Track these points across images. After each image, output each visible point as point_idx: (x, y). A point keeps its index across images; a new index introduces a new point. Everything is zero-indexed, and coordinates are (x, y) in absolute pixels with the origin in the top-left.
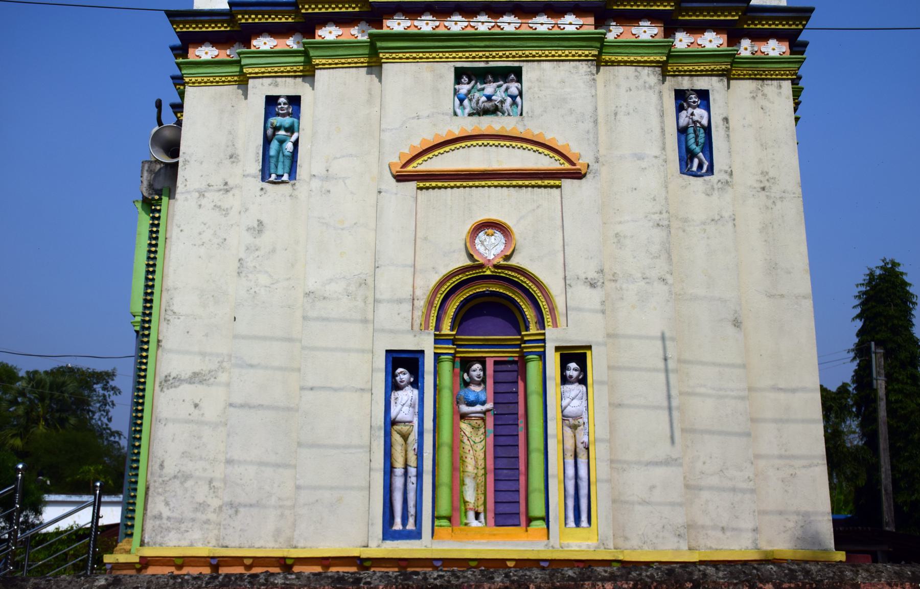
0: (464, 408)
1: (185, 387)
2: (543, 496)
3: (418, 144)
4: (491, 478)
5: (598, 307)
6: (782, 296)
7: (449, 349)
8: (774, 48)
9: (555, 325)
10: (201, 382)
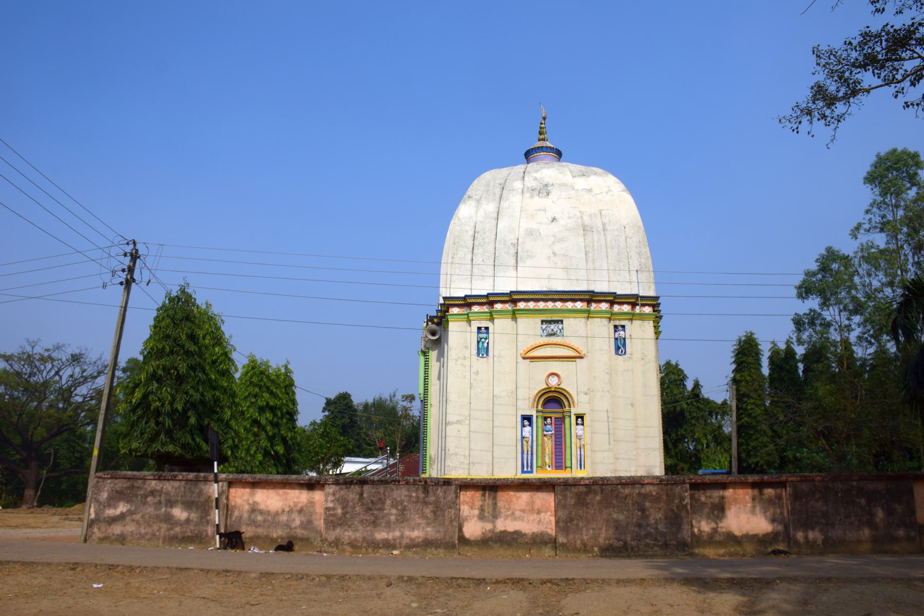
0: (545, 433)
6: (648, 395)
7: (541, 414)
8: (648, 310)
9: (574, 407)
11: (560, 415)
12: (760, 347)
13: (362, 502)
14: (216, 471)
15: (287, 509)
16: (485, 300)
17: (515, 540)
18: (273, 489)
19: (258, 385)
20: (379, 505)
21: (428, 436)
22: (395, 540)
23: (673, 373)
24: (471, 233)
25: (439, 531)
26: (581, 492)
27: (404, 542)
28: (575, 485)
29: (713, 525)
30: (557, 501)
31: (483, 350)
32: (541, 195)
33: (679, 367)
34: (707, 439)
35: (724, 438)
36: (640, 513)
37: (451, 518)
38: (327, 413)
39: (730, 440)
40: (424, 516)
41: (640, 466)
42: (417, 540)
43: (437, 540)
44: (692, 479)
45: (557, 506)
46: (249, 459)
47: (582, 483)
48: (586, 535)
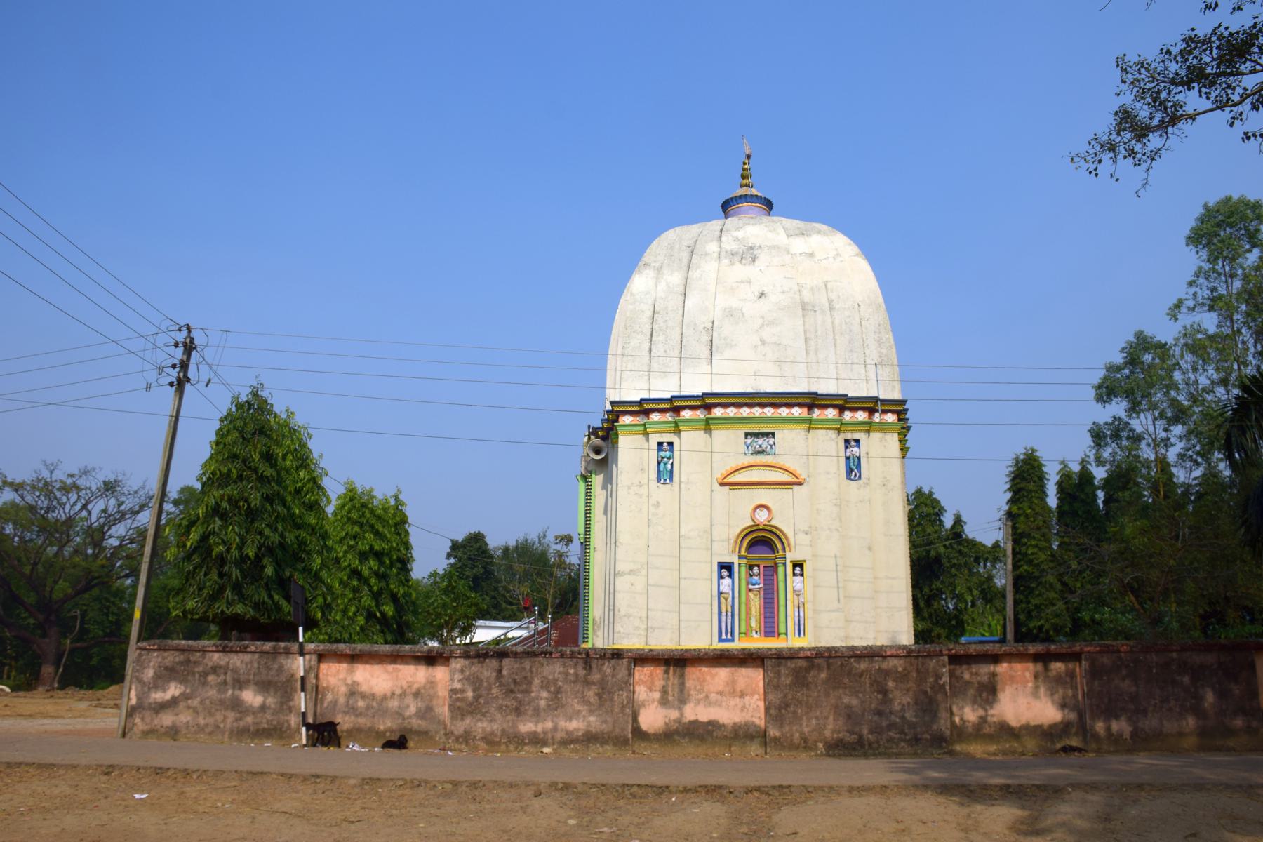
0: (751, 587)
3: (729, 468)
4: (762, 617)
6: (891, 535)
7: (744, 561)
8: (891, 418)
9: (790, 551)
11: (770, 563)
12: (1044, 469)
13: (501, 682)
14: (301, 639)
15: (398, 692)
16: (667, 406)
17: (710, 733)
20: (525, 686)
22: (545, 733)
23: (926, 505)
24: (649, 314)
25: (605, 722)
26: (800, 668)
27: (559, 736)
29: (981, 712)
30: (767, 681)
31: (665, 474)
32: (744, 261)
33: (934, 496)
34: (972, 596)
36: (880, 696)
38: (452, 561)
39: (1004, 596)
40: (585, 701)
43: (603, 733)
44: (952, 649)
46: (346, 623)
47: (801, 655)
48: (807, 726)
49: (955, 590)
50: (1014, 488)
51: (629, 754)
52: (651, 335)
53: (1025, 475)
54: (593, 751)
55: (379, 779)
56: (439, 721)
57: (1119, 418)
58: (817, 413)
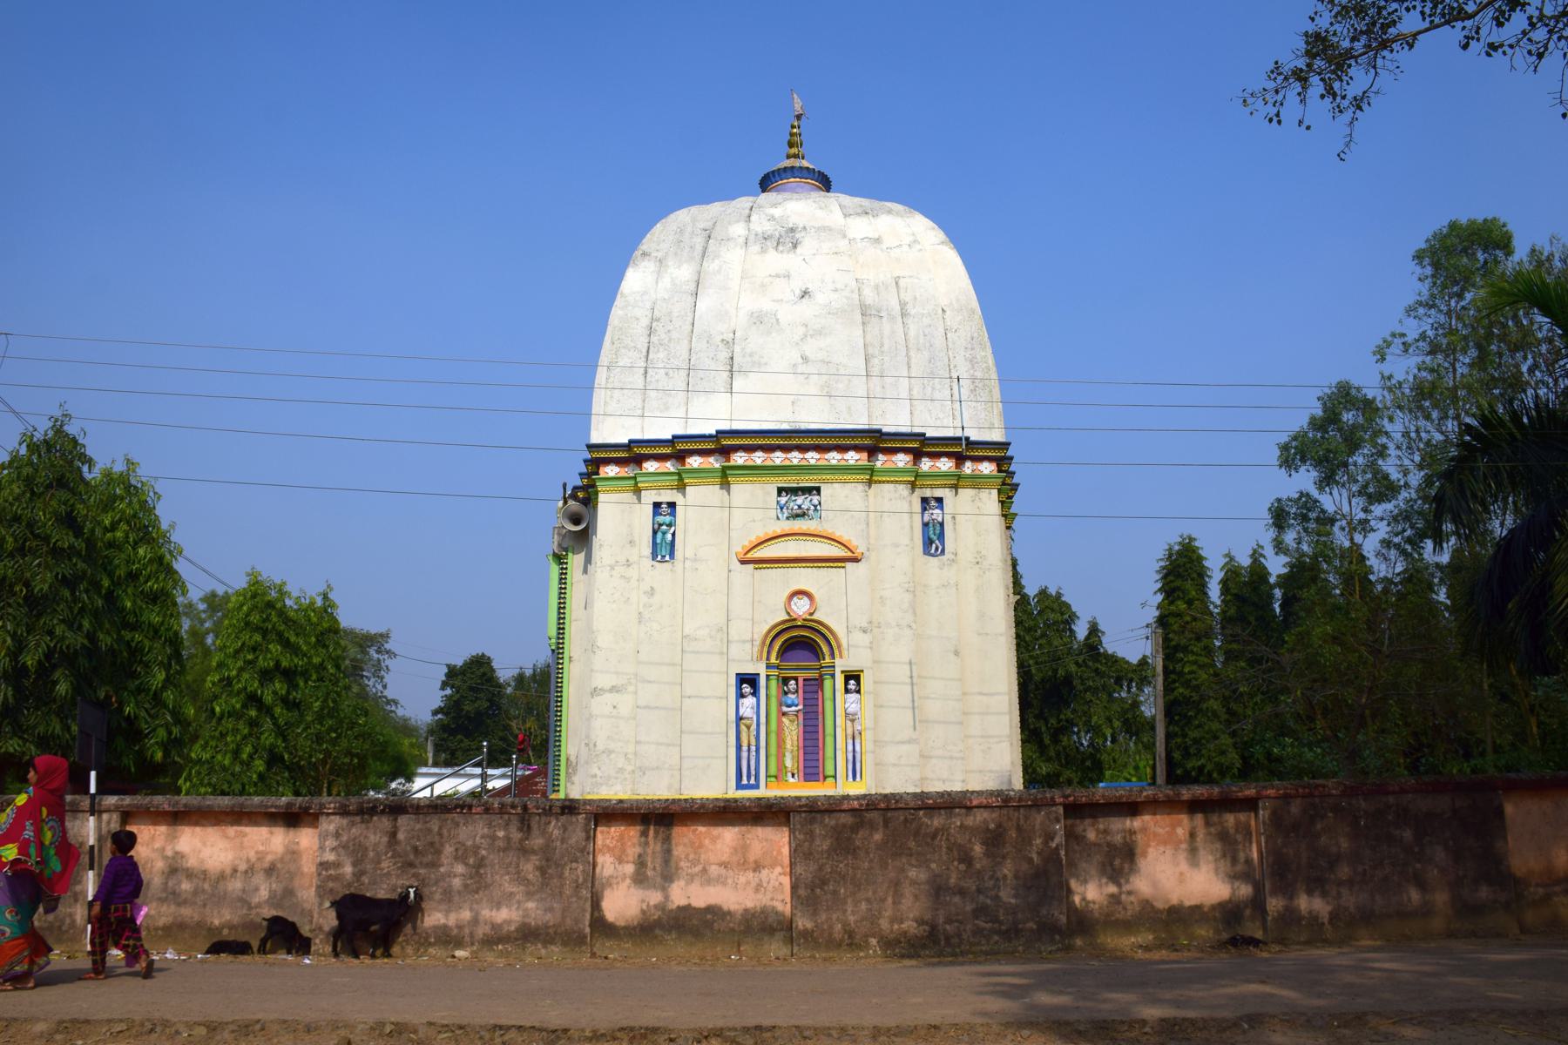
0: (785, 709)
1: (607, 695)
2: (833, 762)
4: (801, 752)
5: (868, 645)
6: (987, 634)
7: (775, 672)
8: (987, 468)
9: (841, 657)
10: (617, 692)
11: (813, 674)
12: (1206, 563)
13: (394, 850)
14: (93, 790)
15: (243, 867)
16: (668, 450)
17: (709, 925)
18: (215, 825)
19: (262, 628)
20: (430, 857)
21: (564, 718)
22: (460, 927)
23: (1053, 610)
24: (645, 322)
25: (551, 909)
26: (844, 826)
27: (481, 931)
28: (830, 811)
29: (1112, 889)
30: (793, 845)
31: (663, 547)
32: (781, 248)
33: (1063, 599)
34: (1112, 728)
35: (1143, 725)
36: (962, 867)
37: (577, 881)
38: (448, 691)
39: (1153, 728)
40: (520, 879)
41: (972, 771)
42: (506, 928)
43: (548, 928)
44: (1069, 796)
45: (794, 853)
46: (238, 769)
47: (845, 807)
48: (853, 913)
49: (1090, 722)
50: (1167, 588)
51: (585, 959)
52: (648, 352)
53: (1181, 570)
54: (531, 954)
55: (87, 1022)
56: (303, 910)
57: (1308, 494)
58: (881, 460)
